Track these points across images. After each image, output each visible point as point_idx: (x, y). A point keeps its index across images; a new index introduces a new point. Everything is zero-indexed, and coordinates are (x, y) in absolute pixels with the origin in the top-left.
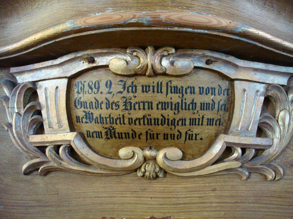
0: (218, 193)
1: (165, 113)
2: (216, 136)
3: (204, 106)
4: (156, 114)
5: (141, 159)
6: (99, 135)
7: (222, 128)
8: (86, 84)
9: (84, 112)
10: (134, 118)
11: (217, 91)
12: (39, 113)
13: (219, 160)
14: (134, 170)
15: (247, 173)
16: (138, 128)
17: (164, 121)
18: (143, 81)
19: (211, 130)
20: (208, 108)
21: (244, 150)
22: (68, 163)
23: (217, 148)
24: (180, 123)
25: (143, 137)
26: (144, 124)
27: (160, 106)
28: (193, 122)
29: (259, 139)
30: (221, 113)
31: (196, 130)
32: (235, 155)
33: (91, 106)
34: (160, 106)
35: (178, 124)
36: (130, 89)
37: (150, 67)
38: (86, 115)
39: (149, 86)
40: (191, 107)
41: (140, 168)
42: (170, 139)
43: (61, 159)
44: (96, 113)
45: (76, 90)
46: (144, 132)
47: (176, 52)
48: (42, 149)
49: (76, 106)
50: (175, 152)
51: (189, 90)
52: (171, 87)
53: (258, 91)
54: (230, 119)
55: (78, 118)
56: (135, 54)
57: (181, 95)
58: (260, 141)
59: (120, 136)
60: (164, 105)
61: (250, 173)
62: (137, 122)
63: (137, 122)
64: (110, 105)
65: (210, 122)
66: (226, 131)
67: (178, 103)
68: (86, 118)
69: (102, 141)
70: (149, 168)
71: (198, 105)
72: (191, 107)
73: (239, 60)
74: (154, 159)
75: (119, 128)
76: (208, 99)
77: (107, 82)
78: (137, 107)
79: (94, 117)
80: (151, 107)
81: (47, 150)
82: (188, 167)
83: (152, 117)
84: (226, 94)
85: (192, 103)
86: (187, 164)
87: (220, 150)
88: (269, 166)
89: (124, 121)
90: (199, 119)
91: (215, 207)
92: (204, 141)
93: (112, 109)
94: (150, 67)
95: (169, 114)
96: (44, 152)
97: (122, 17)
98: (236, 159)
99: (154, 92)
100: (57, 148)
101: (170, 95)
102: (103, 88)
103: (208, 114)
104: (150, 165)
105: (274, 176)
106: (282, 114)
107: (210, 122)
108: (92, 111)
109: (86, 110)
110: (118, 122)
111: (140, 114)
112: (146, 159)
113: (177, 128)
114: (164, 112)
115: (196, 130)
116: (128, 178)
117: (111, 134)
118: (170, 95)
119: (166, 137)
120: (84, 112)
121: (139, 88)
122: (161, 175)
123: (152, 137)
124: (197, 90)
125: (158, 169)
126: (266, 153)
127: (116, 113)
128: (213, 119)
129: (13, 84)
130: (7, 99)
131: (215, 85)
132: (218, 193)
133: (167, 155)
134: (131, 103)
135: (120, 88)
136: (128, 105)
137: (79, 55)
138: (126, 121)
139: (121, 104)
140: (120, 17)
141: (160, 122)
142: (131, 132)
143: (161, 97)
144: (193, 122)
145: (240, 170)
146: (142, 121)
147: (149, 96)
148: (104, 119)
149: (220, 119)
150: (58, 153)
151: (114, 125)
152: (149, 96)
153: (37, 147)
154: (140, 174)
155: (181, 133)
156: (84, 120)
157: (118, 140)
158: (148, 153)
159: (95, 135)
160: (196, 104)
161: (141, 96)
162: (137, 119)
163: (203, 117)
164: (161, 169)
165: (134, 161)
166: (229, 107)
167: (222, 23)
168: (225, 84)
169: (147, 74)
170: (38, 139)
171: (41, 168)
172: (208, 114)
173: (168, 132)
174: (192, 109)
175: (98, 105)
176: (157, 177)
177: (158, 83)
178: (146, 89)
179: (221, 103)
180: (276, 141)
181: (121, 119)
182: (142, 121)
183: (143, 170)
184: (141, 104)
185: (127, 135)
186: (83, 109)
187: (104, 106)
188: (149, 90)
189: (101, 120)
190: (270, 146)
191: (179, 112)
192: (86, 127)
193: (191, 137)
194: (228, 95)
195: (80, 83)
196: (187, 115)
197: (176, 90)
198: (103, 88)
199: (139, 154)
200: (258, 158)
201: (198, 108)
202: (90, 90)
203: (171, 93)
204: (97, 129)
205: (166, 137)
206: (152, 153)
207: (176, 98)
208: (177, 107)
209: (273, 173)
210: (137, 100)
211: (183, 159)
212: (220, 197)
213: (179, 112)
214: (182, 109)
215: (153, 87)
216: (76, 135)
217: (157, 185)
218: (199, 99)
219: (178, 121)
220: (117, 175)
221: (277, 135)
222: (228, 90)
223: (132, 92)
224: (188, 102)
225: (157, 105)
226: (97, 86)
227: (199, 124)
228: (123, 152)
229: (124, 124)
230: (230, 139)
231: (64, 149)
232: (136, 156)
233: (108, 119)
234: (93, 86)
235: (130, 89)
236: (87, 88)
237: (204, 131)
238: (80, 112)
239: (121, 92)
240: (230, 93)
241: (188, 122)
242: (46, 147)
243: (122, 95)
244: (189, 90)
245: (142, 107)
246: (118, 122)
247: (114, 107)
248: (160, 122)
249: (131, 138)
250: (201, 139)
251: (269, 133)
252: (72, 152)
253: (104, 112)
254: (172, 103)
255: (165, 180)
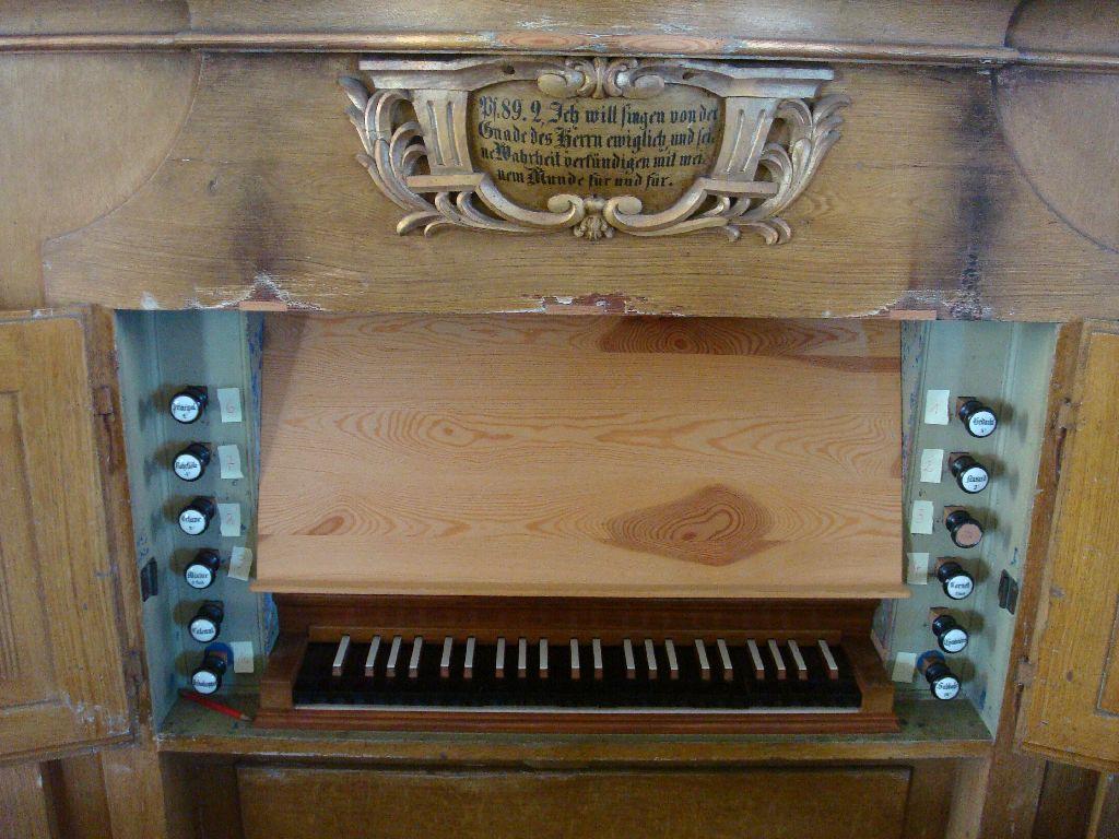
0: (693, 260)
1: (618, 150)
2: (694, 179)
3: (679, 140)
4: (606, 152)
5: (581, 212)
6: (519, 177)
7: (702, 167)
8: (499, 104)
9: (496, 143)
10: (573, 157)
11: (697, 115)
12: (418, 140)
13: (698, 213)
14: (571, 228)
15: (736, 234)
16: (577, 171)
17: (616, 162)
18: (588, 104)
19: (685, 172)
20: (682, 142)
21: (733, 200)
22: (473, 219)
23: (693, 200)
24: (641, 164)
25: (586, 183)
26: (588, 166)
27: (612, 143)
28: (659, 162)
29: (758, 184)
30: (702, 146)
31: (663, 172)
32: (720, 208)
33: (508, 136)
34: (612, 143)
35: (637, 166)
36: (569, 116)
37: (599, 88)
38: (498, 148)
39: (597, 113)
40: (657, 142)
41: (579, 225)
42: (623, 185)
43: (458, 211)
44: (515, 147)
45: (482, 109)
46: (587, 177)
47: (614, 237)
48: (429, 197)
49: (481, 133)
50: (632, 203)
51: (655, 118)
52: (630, 114)
53: (763, 111)
54: (716, 153)
55: (484, 152)
56: (578, 68)
57: (643, 126)
58: (760, 188)
59: (551, 180)
60: (618, 141)
61: (741, 232)
62: (578, 164)
63: (578, 164)
64: (538, 138)
65: (685, 160)
66: (707, 175)
67: (639, 137)
68: (499, 152)
69: (522, 186)
70: (594, 224)
71: (669, 138)
72: (657, 142)
73: (735, 69)
74: (601, 212)
75: (549, 170)
76: (682, 128)
77: (533, 104)
78: (578, 143)
79: (512, 153)
80: (598, 143)
81: (437, 200)
82: (649, 225)
83: (600, 157)
84: (711, 118)
85: (659, 136)
86: (649, 221)
87: (698, 201)
88: (770, 224)
89: (558, 161)
90: (669, 158)
91: (687, 280)
92: (675, 187)
93: (541, 143)
94: (599, 88)
95: (625, 152)
96: (433, 203)
97: (568, 42)
98: (721, 214)
99: (604, 121)
100: (452, 197)
101: (627, 125)
102: (527, 112)
103: (683, 150)
104: (594, 220)
105: (776, 237)
106: (799, 145)
107: (685, 160)
108: (508, 143)
109: (498, 141)
110: (549, 161)
111: (583, 153)
112: (588, 212)
113: (636, 171)
114: (618, 150)
115: (663, 172)
116: (562, 238)
117: (537, 177)
118: (627, 125)
119: (618, 182)
120: (496, 143)
121: (583, 115)
122: (609, 235)
123: (598, 182)
124: (668, 117)
125: (605, 226)
126: (767, 205)
127: (546, 150)
128: (690, 157)
129: (368, 91)
130: (359, 115)
131: (696, 107)
132: (693, 260)
133: (620, 207)
134: (569, 137)
135: (553, 114)
136: (565, 139)
137: (489, 62)
138: (562, 161)
139: (555, 138)
140: (564, 42)
141: (611, 164)
142: (567, 177)
143: (614, 129)
144: (659, 162)
145: (728, 228)
146: (585, 163)
147: (597, 128)
148: (528, 157)
149: (701, 156)
150: (455, 204)
151: (543, 167)
152: (597, 128)
153: (421, 195)
154: (578, 233)
155: (641, 178)
156: (495, 155)
157: (547, 186)
158: (591, 203)
159: (511, 177)
160: (664, 137)
161: (584, 128)
162: (577, 160)
163: (674, 156)
164: (609, 225)
165: (570, 216)
166: (716, 136)
167: (704, 46)
168: (710, 104)
169: (594, 96)
170: (422, 182)
171: (428, 227)
172: (683, 150)
173: (624, 176)
174: (660, 144)
175: (519, 136)
176: (604, 236)
177: (610, 108)
178: (591, 117)
179: (703, 133)
180: (783, 188)
181: (555, 159)
182: (585, 163)
183: (583, 228)
184: (585, 140)
185: (561, 180)
186: (493, 139)
187: (528, 138)
188: (597, 119)
189: (522, 157)
190: (774, 195)
191: (639, 149)
192: (498, 165)
193: (656, 183)
194: (715, 118)
195: (488, 100)
196: (651, 153)
197: (636, 118)
198: (527, 112)
199: (578, 202)
200: (755, 210)
201: (668, 143)
202: (506, 114)
203: (629, 122)
204: (515, 170)
205: (618, 182)
206: (599, 204)
207: (635, 130)
208: (637, 143)
209: (775, 233)
210: (579, 133)
211: (643, 212)
212: (695, 265)
213: (639, 149)
214: (644, 145)
215: (603, 113)
216: (484, 179)
217: (602, 249)
218: (670, 129)
219: (652, 116)
220: (543, 235)
221: (787, 178)
222: (715, 112)
223: (572, 121)
224: (654, 134)
225: (608, 141)
226: (517, 108)
227: (668, 165)
228: (554, 201)
229: (558, 164)
230: (712, 185)
231: (464, 199)
232: (573, 213)
233: (534, 158)
234: (510, 108)
235: (569, 116)
236: (500, 109)
237: (679, 173)
238: (489, 143)
239: (555, 121)
240: (718, 116)
241: (652, 164)
242: (434, 194)
243: (556, 125)
244: (655, 118)
245: (585, 144)
246: (549, 161)
247: (544, 141)
248: (611, 164)
249: (569, 183)
250: (671, 184)
251: (774, 175)
252: (475, 200)
253: (528, 147)
254: (629, 137)
255: (615, 241)
